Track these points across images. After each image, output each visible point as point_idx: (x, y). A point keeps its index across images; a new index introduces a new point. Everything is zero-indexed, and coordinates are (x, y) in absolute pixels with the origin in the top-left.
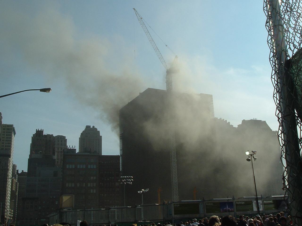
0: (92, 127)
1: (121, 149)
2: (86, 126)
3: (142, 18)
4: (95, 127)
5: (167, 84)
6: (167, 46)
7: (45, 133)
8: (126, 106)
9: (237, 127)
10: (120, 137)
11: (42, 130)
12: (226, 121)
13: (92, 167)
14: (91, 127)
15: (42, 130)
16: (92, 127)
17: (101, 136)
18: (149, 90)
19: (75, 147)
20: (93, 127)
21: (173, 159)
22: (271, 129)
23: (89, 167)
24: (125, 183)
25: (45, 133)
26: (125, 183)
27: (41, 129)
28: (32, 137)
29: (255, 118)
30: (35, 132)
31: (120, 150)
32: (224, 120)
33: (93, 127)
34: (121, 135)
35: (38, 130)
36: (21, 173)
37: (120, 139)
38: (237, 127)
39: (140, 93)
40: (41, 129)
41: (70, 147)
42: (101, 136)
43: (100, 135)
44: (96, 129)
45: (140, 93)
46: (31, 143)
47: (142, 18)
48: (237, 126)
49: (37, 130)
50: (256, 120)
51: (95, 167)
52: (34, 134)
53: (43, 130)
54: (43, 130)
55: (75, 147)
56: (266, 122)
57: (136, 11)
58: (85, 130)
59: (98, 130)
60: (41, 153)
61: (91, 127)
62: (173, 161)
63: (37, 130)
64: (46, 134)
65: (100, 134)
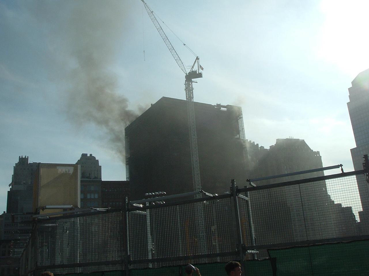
0: (89, 156)
1: (128, 177)
2: (82, 155)
3: (153, 12)
4: (93, 156)
5: (186, 92)
6: (185, 45)
7: (30, 161)
8: (135, 121)
9: (268, 148)
10: (126, 162)
11: (27, 158)
12: (254, 142)
13: (92, 197)
14: (88, 155)
15: (27, 158)
16: (89, 156)
17: (101, 166)
18: (164, 99)
19: (69, 172)
20: (91, 155)
21: (196, 185)
22: (311, 149)
23: (89, 197)
24: (154, 203)
25: (30, 161)
26: (154, 203)
27: (26, 156)
28: (14, 167)
29: (292, 137)
30: (17, 161)
31: (126, 178)
32: (251, 142)
33: (91, 155)
34: (127, 163)
35: (21, 157)
36: (2, 215)
37: (126, 164)
38: (269, 148)
39: (152, 104)
40: (26, 156)
41: (62, 171)
42: (101, 166)
43: (99, 165)
44: (94, 158)
45: (152, 104)
46: (13, 174)
47: (153, 12)
48: (269, 147)
49: (20, 157)
50: (291, 138)
51: (96, 196)
52: (17, 163)
53: (28, 157)
54: (28, 157)
55: (69, 172)
56: (305, 141)
57: (146, 4)
58: (80, 159)
59: (96, 159)
60: (24, 183)
61: (88, 155)
62: (197, 189)
63: (20, 157)
64: (32, 163)
65: (99, 163)
